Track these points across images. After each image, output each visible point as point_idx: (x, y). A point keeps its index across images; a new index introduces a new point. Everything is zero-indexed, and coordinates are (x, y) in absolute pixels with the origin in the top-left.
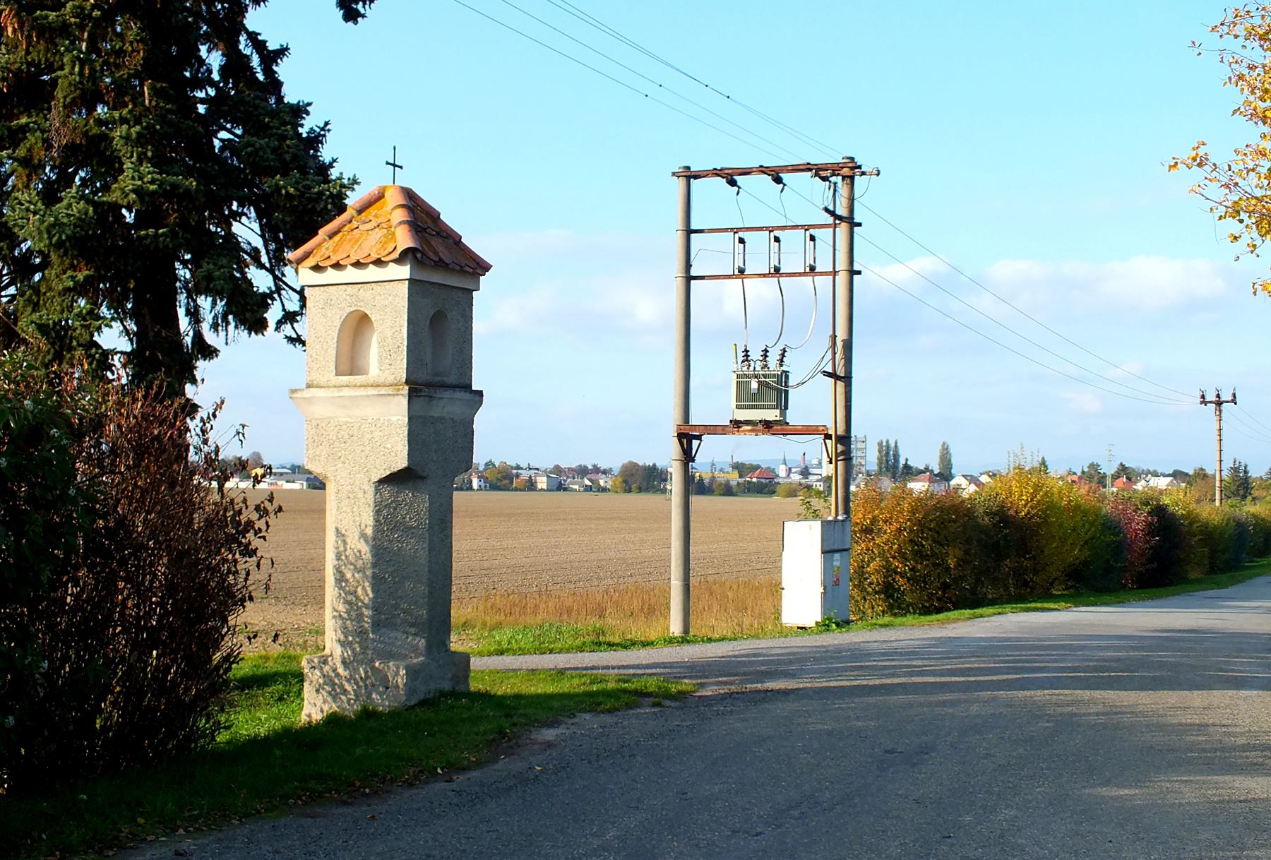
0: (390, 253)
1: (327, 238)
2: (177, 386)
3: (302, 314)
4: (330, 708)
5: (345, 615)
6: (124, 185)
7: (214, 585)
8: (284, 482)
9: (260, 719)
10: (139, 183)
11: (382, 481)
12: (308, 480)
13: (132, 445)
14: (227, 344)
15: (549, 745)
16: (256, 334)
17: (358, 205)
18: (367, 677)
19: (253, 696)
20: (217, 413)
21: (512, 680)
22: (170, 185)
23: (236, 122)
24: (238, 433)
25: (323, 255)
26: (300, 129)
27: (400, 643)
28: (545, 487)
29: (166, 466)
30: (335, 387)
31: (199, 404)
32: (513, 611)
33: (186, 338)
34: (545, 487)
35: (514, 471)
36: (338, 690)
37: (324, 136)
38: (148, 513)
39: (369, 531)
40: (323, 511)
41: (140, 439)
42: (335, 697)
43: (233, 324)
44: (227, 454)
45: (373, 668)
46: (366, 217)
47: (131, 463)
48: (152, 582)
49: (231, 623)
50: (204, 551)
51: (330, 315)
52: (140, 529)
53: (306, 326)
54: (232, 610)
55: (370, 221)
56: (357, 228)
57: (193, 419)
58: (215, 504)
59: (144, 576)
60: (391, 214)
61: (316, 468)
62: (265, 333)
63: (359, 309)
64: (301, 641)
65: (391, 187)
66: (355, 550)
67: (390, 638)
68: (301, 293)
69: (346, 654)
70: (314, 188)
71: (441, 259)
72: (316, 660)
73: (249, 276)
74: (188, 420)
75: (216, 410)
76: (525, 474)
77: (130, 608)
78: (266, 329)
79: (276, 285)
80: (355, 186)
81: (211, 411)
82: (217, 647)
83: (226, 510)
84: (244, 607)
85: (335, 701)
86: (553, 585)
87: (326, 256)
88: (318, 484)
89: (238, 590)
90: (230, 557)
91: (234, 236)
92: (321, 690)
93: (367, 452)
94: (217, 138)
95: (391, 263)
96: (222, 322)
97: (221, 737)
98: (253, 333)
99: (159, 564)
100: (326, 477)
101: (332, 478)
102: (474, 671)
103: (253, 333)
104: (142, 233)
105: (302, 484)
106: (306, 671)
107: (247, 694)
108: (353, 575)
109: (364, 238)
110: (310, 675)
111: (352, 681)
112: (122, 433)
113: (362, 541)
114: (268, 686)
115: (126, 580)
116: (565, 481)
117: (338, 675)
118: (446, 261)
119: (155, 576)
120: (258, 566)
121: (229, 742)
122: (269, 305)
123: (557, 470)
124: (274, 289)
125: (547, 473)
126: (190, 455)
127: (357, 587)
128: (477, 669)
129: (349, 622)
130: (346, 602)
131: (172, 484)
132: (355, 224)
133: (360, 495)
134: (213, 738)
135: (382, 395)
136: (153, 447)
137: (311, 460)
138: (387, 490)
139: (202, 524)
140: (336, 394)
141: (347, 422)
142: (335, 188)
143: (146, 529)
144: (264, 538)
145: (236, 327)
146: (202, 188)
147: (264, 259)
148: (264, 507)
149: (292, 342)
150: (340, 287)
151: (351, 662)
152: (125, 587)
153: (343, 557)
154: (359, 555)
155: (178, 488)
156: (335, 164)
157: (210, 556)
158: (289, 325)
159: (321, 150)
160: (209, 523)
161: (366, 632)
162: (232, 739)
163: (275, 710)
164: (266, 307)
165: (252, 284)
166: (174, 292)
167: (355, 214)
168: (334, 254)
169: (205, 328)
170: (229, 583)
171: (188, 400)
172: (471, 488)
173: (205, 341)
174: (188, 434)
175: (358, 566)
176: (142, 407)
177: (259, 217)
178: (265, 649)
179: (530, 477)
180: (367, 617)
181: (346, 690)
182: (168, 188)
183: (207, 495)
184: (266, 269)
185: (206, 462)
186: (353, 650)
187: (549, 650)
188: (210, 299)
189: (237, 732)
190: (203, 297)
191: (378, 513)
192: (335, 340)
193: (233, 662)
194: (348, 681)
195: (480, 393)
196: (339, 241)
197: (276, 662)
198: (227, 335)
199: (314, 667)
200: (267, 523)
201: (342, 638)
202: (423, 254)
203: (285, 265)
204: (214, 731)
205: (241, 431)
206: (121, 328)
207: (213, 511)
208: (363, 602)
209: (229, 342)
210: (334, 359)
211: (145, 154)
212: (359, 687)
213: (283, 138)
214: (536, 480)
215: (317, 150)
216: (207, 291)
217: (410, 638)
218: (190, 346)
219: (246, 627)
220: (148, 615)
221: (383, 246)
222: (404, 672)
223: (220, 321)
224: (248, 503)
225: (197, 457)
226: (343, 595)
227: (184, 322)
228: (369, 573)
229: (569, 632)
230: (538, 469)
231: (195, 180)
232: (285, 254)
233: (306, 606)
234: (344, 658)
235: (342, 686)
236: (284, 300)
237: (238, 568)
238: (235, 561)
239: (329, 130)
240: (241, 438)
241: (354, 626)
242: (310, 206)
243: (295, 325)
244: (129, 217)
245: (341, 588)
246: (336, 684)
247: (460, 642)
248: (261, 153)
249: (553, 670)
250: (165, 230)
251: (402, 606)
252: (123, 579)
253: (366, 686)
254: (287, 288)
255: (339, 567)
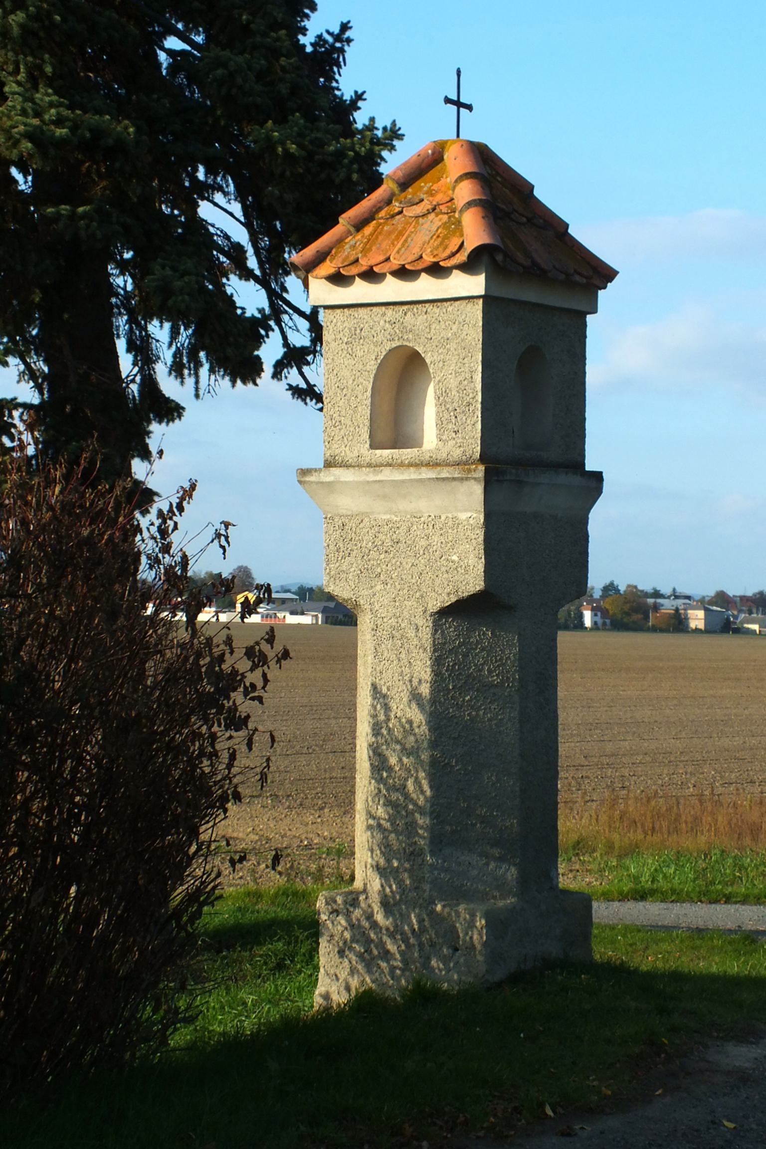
0: (454, 254)
1: (352, 229)
2: (118, 461)
3: (314, 352)
4: (363, 982)
5: (387, 825)
6: (9, 123)
7: (177, 774)
8: (288, 615)
9: (244, 1004)
10: (36, 122)
11: (444, 613)
12: (324, 611)
13: (46, 553)
14: (197, 396)
15: (743, 1078)
16: (244, 382)
17: (400, 174)
18: (423, 930)
19: (235, 961)
20: (185, 504)
21: (665, 946)
22: (91, 130)
23: (193, 20)
24: (218, 535)
25: (347, 257)
26: (300, 37)
27: (475, 872)
28: (701, 625)
29: (103, 586)
30: (369, 465)
31: (155, 489)
32: (657, 826)
33: (131, 386)
34: (701, 625)
35: (651, 601)
36: (375, 952)
37: (342, 51)
38: (72, 659)
39: (425, 690)
40: (354, 658)
41: (59, 542)
42: (369, 963)
43: (206, 366)
44: (199, 568)
45: (432, 913)
46: (414, 194)
47: (45, 581)
48: (74, 771)
49: (204, 837)
50: (162, 720)
51: (360, 354)
52: (57, 685)
53: (321, 370)
54: (206, 815)
55: (423, 200)
56: (401, 212)
57: (145, 512)
58: (182, 646)
59: (62, 762)
60: (454, 189)
61: (341, 591)
62: (258, 381)
63: (405, 343)
64: (313, 867)
65: (453, 142)
66: (404, 720)
67: (459, 864)
68: (312, 318)
69: (388, 890)
70: (329, 145)
71: (535, 263)
72: (339, 899)
73: (229, 290)
74: (137, 515)
75: (182, 499)
76: (668, 606)
77: (35, 815)
78: (259, 375)
79: (272, 304)
80: (396, 142)
81: (175, 501)
82: (179, 875)
83: (199, 655)
84: (226, 811)
85: (369, 971)
86: (722, 785)
87: (352, 258)
88: (341, 617)
89: (216, 783)
90: (204, 729)
91: (202, 224)
92: (347, 953)
93: (421, 567)
94: (163, 49)
95: (455, 272)
96: (189, 362)
97: (177, 1038)
98: (239, 382)
99: (88, 742)
100: (357, 605)
101: (367, 606)
102: (599, 926)
103: (239, 382)
104: (49, 210)
105: (316, 616)
106: (324, 917)
107: (225, 957)
108: (400, 760)
109: (411, 229)
110: (330, 925)
111: (399, 937)
112: (29, 532)
113: (414, 705)
114: (260, 944)
115: (31, 767)
116: (736, 617)
117: (375, 925)
118: (544, 266)
119: (80, 760)
120: (250, 745)
121: (191, 1047)
122: (262, 337)
123: (722, 598)
124: (267, 311)
125: (703, 604)
126: (141, 568)
127: (406, 780)
128: (605, 921)
129: (393, 835)
130: (388, 803)
131: (113, 615)
132: (396, 206)
133: (411, 633)
134: (164, 1041)
135: (444, 479)
136: (81, 556)
137: (334, 578)
138: (452, 627)
139: (160, 677)
140: (372, 478)
141: (389, 521)
142: (363, 145)
143: (67, 686)
144: (260, 699)
145: (212, 371)
146: (145, 138)
147: (252, 263)
148: (260, 650)
149: (300, 396)
150: (375, 309)
151: (397, 904)
152: (29, 779)
153: (384, 732)
154: (409, 728)
155: (121, 621)
156: (360, 104)
157: (171, 729)
158: (295, 368)
159: (337, 77)
160: (172, 675)
161: (421, 853)
162: (195, 1042)
163: (269, 986)
164: (258, 341)
165: (234, 302)
166: (108, 314)
167: (397, 190)
168: (365, 256)
169: (161, 372)
170: (203, 772)
171: (137, 483)
172: (580, 626)
173: (160, 391)
174: (138, 538)
175: (408, 746)
176: (61, 492)
177: (241, 196)
178: (255, 880)
179: (677, 610)
180: (422, 827)
181: (387, 952)
182: (88, 135)
183: (168, 631)
184: (257, 280)
185: (167, 580)
186: (400, 883)
187: (725, 895)
188: (167, 325)
189: (204, 1029)
190: (156, 322)
191: (438, 662)
192: (369, 394)
193: (205, 903)
194: (392, 935)
195: (598, 477)
196: (372, 234)
197: (273, 903)
198: (197, 382)
199: (336, 912)
200: (264, 675)
201: (382, 862)
202: (506, 255)
203: (287, 273)
204: (165, 1028)
205: (223, 532)
206: (22, 367)
207: (179, 656)
208: (415, 804)
209: (201, 393)
210: (367, 423)
211: (40, 68)
212: (408, 946)
213: (274, 53)
214: (686, 615)
215: (330, 78)
216: (163, 314)
217: (492, 865)
218: (136, 394)
219: (228, 844)
220: (67, 825)
221: (441, 243)
222: (483, 922)
223: (185, 360)
224: (234, 645)
225: (153, 573)
226: (384, 792)
227: (126, 363)
228: (425, 756)
229: (757, 868)
230: (688, 598)
231: (134, 125)
232: (286, 256)
233: (322, 809)
234: (386, 896)
235: (381, 945)
236: (286, 329)
237: (218, 747)
238: (213, 737)
239: (349, 41)
240: (223, 542)
241: (401, 842)
242: (323, 176)
243: (305, 369)
244: (23, 182)
245: (380, 780)
246: (372, 941)
247: (570, 876)
248: (239, 81)
249: (735, 932)
250: (87, 208)
251: (478, 812)
252: (26, 766)
253: (421, 945)
254: (291, 312)
255: (378, 747)
